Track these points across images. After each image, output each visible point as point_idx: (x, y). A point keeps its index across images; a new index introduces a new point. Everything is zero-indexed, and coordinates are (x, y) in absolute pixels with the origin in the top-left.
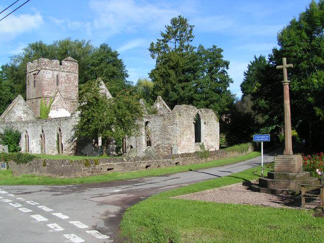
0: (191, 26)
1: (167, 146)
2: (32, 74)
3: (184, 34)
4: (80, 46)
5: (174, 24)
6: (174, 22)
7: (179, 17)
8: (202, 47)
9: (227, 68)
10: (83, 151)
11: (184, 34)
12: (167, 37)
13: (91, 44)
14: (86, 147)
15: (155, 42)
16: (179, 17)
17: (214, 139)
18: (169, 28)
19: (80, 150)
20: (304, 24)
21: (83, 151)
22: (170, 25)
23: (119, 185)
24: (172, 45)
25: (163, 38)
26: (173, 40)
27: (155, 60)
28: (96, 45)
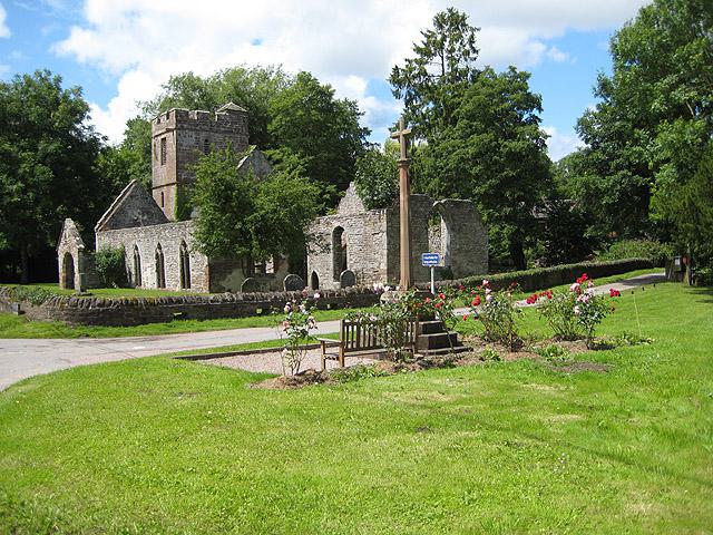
0: (473, 30)
1: (371, 273)
2: (159, 138)
3: (457, 46)
4: (264, 77)
5: (441, 27)
6: (440, 21)
7: (450, 11)
8: (492, 71)
9: (540, 110)
10: (223, 284)
11: (457, 46)
12: (425, 53)
13: (285, 70)
14: (229, 276)
15: (402, 65)
16: (450, 11)
17: (475, 258)
18: (127, 132)
19: (218, 280)
20: (191, 139)
21: (223, 284)
22: (433, 29)
23: (144, 321)
24: (435, 68)
25: (419, 57)
26: (437, 59)
27: (402, 101)
28: (292, 71)
